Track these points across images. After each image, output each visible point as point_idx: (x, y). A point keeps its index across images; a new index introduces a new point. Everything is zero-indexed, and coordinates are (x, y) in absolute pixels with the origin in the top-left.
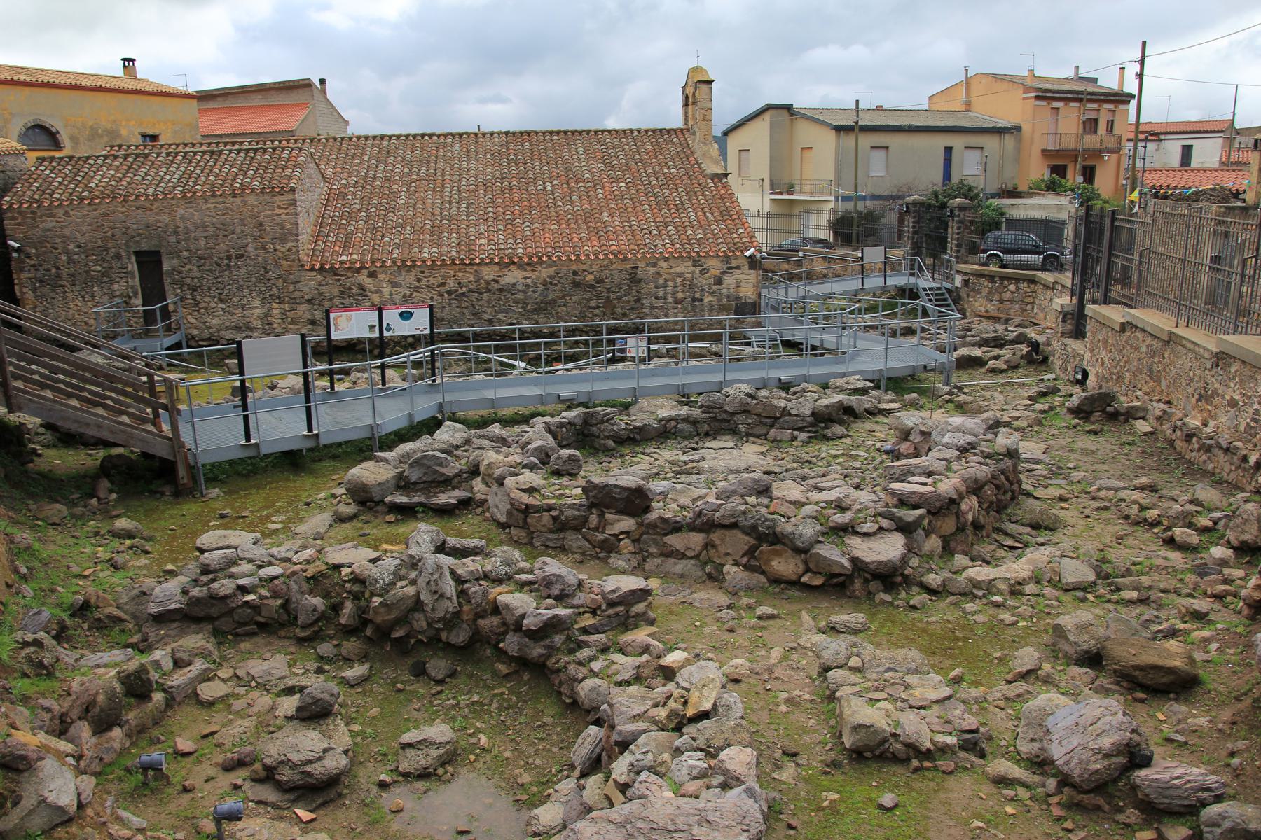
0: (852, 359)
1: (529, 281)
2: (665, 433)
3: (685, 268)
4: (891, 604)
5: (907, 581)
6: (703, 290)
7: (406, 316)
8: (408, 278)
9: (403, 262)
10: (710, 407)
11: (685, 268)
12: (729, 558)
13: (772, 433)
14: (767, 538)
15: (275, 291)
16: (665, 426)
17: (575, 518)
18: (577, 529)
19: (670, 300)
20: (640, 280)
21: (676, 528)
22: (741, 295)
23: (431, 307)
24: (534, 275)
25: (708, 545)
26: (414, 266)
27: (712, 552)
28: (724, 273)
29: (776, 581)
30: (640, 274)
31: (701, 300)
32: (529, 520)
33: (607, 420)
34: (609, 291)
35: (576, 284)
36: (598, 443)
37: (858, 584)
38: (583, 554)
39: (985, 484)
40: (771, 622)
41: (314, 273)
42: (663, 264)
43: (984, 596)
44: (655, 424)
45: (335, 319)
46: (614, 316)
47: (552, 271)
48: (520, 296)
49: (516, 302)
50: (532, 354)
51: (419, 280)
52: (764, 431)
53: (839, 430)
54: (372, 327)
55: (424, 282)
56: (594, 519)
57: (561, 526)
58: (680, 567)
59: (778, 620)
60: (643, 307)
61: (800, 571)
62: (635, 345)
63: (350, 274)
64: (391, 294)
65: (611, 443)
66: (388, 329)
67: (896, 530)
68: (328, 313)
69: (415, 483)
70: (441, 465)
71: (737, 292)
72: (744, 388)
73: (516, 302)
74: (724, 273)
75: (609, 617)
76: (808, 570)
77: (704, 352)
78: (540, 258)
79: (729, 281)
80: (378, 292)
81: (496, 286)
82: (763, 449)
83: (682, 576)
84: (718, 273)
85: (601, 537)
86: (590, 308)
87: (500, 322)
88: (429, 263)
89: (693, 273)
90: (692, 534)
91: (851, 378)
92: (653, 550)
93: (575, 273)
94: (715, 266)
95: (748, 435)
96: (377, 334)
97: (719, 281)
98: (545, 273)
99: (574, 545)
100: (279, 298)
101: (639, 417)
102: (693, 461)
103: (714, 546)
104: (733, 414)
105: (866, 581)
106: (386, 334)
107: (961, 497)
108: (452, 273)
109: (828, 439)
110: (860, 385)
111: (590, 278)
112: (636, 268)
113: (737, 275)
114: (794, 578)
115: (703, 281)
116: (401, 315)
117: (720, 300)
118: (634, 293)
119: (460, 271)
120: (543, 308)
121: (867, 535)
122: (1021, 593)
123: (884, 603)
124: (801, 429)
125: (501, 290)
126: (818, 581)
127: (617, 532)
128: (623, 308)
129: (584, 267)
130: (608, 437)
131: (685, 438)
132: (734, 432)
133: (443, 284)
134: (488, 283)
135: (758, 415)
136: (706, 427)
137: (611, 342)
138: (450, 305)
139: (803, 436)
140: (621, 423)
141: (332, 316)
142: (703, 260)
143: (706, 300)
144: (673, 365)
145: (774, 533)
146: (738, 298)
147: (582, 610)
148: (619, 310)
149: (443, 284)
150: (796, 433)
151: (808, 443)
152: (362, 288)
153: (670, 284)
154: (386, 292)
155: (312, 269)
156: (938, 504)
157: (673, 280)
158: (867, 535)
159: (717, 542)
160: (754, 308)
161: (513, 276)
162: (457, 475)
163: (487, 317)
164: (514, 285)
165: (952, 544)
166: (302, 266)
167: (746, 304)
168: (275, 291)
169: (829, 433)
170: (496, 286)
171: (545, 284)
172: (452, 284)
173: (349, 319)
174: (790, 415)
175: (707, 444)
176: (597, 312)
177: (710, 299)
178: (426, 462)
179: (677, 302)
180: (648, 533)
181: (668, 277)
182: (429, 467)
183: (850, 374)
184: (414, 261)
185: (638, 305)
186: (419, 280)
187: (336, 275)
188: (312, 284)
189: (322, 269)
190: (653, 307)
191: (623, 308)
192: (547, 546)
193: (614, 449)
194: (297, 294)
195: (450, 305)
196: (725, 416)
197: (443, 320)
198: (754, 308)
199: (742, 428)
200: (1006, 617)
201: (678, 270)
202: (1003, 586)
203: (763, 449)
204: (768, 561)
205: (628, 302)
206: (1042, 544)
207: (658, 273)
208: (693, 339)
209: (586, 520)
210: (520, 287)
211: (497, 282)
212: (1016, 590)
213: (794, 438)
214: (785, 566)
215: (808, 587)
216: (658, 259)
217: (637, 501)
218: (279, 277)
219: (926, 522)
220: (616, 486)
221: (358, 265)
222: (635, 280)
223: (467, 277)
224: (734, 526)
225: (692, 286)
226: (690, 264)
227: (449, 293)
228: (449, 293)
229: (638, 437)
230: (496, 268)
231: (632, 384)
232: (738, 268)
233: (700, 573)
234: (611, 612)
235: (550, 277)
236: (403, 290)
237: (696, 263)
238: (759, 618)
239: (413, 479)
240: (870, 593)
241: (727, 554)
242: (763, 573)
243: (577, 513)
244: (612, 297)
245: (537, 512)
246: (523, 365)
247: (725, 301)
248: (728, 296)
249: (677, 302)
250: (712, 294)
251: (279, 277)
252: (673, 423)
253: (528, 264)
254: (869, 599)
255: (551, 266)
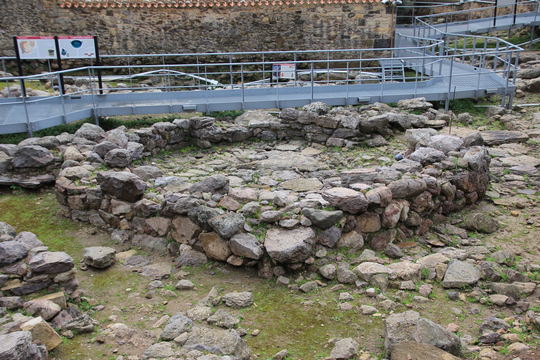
0: (434, 83)
1: (222, 21)
2: (252, 137)
3: (337, 13)
4: (286, 285)
5: (307, 268)
6: (350, 29)
7: (77, 44)
8: (135, 17)
9: (131, 4)
10: (287, 119)
11: (337, 13)
12: (184, 239)
13: (330, 140)
14: (206, 227)
15: (40, 23)
16: (252, 132)
17: (94, 201)
18: (96, 208)
19: (325, 36)
20: (302, 22)
21: (153, 213)
22: (380, 33)
23: (96, 39)
24: (225, 17)
25: (171, 228)
26: (138, 8)
27: (174, 233)
28: (367, 16)
29: (212, 259)
30: (303, 17)
31: (349, 37)
32: (69, 200)
33: (205, 125)
34: (280, 30)
35: (255, 24)
36: (200, 142)
37: (266, 267)
38: (100, 228)
39: (421, 191)
40: (184, 293)
41: (68, 11)
42: (320, 9)
43: (363, 287)
44: (245, 130)
45: (22, 44)
46: (283, 48)
47: (238, 14)
48: (215, 32)
49: (213, 37)
50: (224, 73)
51: (143, 19)
52: (324, 138)
53: (379, 139)
54: (51, 52)
55: (147, 20)
56: (104, 203)
57: (87, 206)
58: (152, 242)
59: (191, 292)
60: (304, 41)
61: (226, 253)
62: (287, 70)
63: (93, 13)
64: (124, 29)
65: (208, 143)
66: (64, 53)
67: (311, 226)
68: (15, 39)
69: (18, 168)
70: (37, 155)
71: (376, 31)
72: (319, 105)
73: (213, 37)
74: (367, 16)
75: (33, 282)
76: (232, 254)
77: (344, 76)
78: (229, 4)
79: (371, 22)
80: (115, 26)
81: (198, 25)
82: (316, 152)
83: (153, 250)
84: (362, 16)
85: (109, 216)
86: (265, 42)
87: (201, 51)
88: (149, 6)
89: (343, 16)
90: (161, 218)
91: (415, 100)
92: (140, 228)
93: (255, 16)
94: (360, 11)
95: (313, 141)
96: (55, 57)
97: (363, 23)
98: (233, 15)
99: (95, 221)
100: (44, 28)
101: (238, 126)
102: (257, 159)
103: (174, 229)
104: (303, 125)
105: (273, 266)
106: (62, 57)
107: (387, 204)
108: (167, 14)
109: (369, 147)
110: (420, 105)
111: (266, 19)
112: (300, 12)
113: (377, 18)
114: (223, 258)
115: (350, 23)
116: (73, 43)
117: (362, 37)
118: (298, 31)
119: (172, 12)
120: (232, 42)
121: (286, 229)
122: (397, 287)
123: (282, 285)
124: (349, 138)
125: (201, 28)
126: (239, 263)
127: (118, 213)
128: (289, 42)
129: (262, 11)
130: (205, 139)
131: (267, 141)
132: (303, 138)
133: (160, 22)
134: (192, 22)
135: (321, 126)
136: (283, 134)
137: (270, 67)
138: (166, 38)
139: (350, 143)
140: (220, 127)
141: (19, 41)
142: (351, 7)
143: (352, 37)
144: (298, 85)
145: (207, 223)
146: (377, 36)
147: (12, 276)
148: (286, 44)
149: (160, 22)
150: (346, 141)
151: (352, 149)
152: (103, 23)
153: (325, 25)
154: (120, 26)
155: (66, 8)
156: (357, 207)
157: (327, 22)
158: (286, 229)
159: (176, 226)
160: (390, 43)
161: (210, 18)
162: (49, 164)
163: (192, 47)
164: (211, 24)
165: (374, 240)
166: (59, 5)
167: (383, 40)
168: (40, 23)
169: (370, 142)
170: (198, 25)
171: (233, 23)
172: (166, 22)
173: (33, 45)
174: (343, 127)
175: (280, 147)
176: (271, 45)
177: (356, 36)
178: (25, 152)
179: (330, 38)
180: (136, 215)
181: (324, 19)
182: (28, 157)
183: (417, 96)
184: (138, 4)
185: (301, 40)
186: (143, 19)
187: (84, 12)
188: (67, 19)
189: (73, 7)
190: (312, 43)
191: (289, 42)
192: (80, 220)
193: (209, 148)
194: (57, 26)
195: (166, 38)
196: (298, 126)
197: (161, 48)
198: (390, 43)
199: (309, 136)
200: (368, 307)
201: (331, 14)
202: (381, 280)
203: (316, 152)
204: (206, 244)
205: (294, 38)
206: (466, 245)
207: (316, 16)
208: (334, 66)
209: (100, 202)
210: (215, 26)
211: (199, 21)
212: (392, 285)
213: (344, 145)
214: (217, 249)
215: (232, 267)
216: (316, 6)
217: (131, 191)
218: (43, 12)
219: (343, 221)
220: (115, 179)
221: (98, 6)
222: (299, 22)
223: (177, 17)
224: (185, 215)
225: (342, 27)
226: (341, 9)
227: (165, 29)
228: (165, 29)
229: (230, 139)
230: (198, 11)
231: (239, 100)
232: (378, 12)
233: (165, 249)
234: (35, 278)
235: (237, 19)
236: (132, 26)
237: (345, 8)
238: (178, 289)
239: (17, 164)
240: (274, 275)
241: (183, 236)
242: (204, 252)
243: (95, 198)
244: (282, 34)
245: (73, 194)
246: (215, 82)
247: (366, 38)
248: (369, 34)
249: (330, 38)
250: (357, 32)
251: (43, 12)
252: (259, 130)
253: (221, 9)
254: (272, 280)
255: (237, 10)
